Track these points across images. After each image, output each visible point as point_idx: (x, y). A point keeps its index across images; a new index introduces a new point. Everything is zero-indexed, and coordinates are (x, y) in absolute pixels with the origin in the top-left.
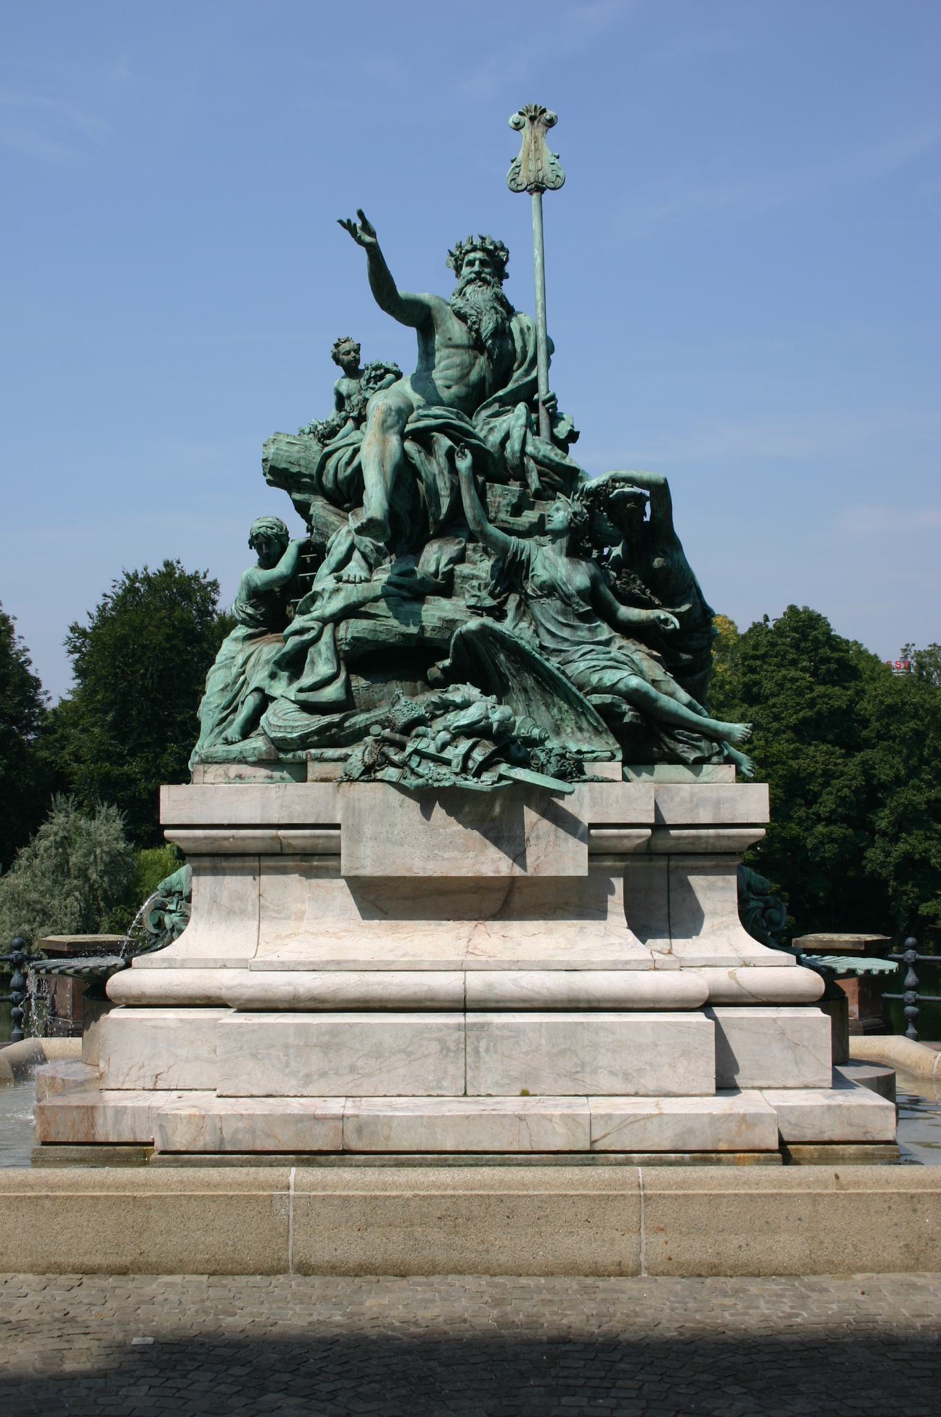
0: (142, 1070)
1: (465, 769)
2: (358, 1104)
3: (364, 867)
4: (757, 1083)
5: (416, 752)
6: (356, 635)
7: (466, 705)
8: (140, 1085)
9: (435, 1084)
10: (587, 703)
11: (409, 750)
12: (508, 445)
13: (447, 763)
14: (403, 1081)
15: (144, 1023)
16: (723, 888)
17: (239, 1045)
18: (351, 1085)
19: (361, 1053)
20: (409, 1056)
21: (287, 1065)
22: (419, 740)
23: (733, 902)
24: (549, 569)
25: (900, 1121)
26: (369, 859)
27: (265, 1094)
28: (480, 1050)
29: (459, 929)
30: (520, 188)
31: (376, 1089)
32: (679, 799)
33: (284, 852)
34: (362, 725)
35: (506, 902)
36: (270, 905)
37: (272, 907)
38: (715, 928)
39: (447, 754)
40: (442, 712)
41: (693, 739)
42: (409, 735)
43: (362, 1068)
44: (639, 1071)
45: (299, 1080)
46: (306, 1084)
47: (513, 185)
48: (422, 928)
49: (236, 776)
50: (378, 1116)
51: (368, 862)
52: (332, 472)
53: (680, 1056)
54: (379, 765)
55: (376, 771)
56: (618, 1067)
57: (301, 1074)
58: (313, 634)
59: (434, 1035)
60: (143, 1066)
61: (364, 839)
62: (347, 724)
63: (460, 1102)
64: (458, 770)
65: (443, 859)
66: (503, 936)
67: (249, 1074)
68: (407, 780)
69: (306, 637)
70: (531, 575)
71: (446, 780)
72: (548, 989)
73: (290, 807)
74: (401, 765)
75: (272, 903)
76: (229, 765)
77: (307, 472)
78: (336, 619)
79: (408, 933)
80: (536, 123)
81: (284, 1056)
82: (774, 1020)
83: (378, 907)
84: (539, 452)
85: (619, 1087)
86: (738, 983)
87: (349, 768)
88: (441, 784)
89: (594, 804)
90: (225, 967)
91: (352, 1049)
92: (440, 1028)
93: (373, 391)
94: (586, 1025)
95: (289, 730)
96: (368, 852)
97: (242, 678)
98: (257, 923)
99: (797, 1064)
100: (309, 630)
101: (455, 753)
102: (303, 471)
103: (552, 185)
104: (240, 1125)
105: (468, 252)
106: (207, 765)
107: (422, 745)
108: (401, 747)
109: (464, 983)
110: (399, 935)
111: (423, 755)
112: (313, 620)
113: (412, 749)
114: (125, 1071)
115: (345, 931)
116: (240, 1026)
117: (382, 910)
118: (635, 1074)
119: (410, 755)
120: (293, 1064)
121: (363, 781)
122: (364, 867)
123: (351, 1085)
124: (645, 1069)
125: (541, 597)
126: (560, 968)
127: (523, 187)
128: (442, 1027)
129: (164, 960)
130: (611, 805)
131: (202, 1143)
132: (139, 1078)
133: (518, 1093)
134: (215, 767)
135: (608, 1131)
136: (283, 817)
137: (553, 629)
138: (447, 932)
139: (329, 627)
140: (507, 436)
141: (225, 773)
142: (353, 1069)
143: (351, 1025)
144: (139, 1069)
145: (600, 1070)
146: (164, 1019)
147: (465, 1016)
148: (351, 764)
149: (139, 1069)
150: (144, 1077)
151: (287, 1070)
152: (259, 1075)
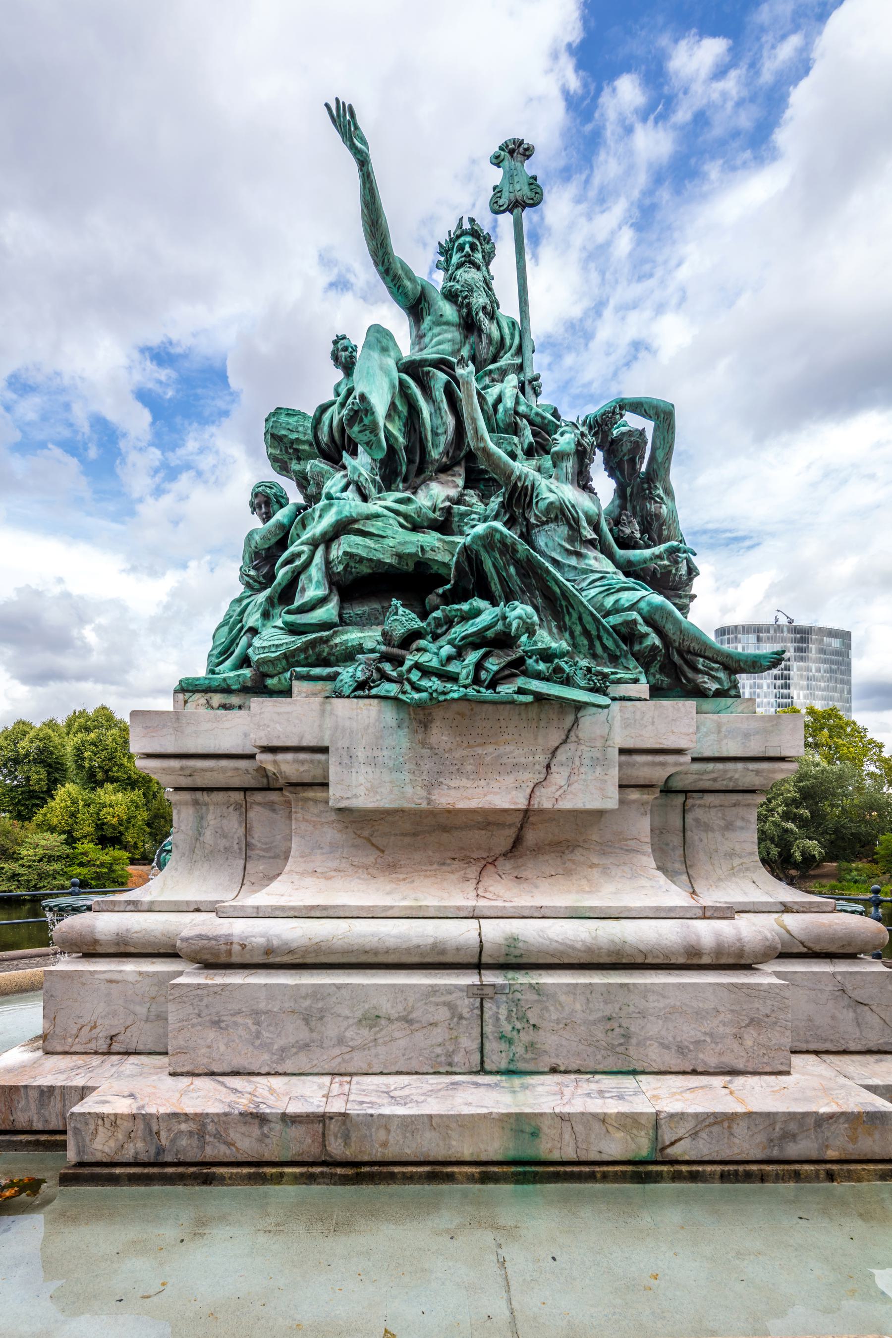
0: (94, 1031)
1: (477, 681)
2: (346, 1087)
3: (356, 796)
4: (812, 1047)
5: (417, 666)
6: (348, 550)
7: (477, 613)
8: (92, 1046)
9: (443, 1059)
10: (606, 624)
11: (408, 664)
12: (501, 408)
13: (453, 678)
14: (404, 1055)
15: (96, 976)
16: (742, 828)
17: (196, 1011)
18: (339, 1059)
19: (351, 1021)
20: (412, 1025)
21: (258, 1035)
22: (419, 654)
23: (753, 842)
24: (556, 491)
25: (487, 1067)
26: (362, 788)
27: (229, 1070)
28: (500, 1016)
29: (466, 868)
30: (502, 208)
31: (370, 1065)
32: (705, 730)
33: (271, 787)
34: (355, 643)
35: (518, 841)
36: (257, 843)
37: (259, 845)
38: (736, 870)
39: (453, 668)
40: (444, 628)
41: (712, 669)
42: (408, 650)
43: (352, 1039)
44: (697, 1043)
45: (273, 1054)
46: (282, 1060)
47: (496, 207)
48: (424, 868)
49: (220, 706)
50: (372, 1115)
51: (361, 791)
52: (327, 423)
53: (748, 1025)
54: (374, 681)
55: (371, 688)
56: (671, 1039)
57: (276, 1047)
58: (304, 557)
59: (443, 999)
60: (95, 1027)
61: (356, 764)
62: (337, 640)
63: (477, 1085)
64: (469, 681)
65: (449, 787)
66: (516, 877)
67: (209, 1047)
68: (407, 695)
69: (298, 563)
70: (534, 501)
71: (454, 691)
72: (582, 941)
73: (268, 726)
74: (399, 681)
75: (259, 841)
76: (212, 695)
77: (305, 439)
78: (329, 539)
79: (407, 873)
80: (515, 155)
81: (254, 1024)
82: (834, 974)
83: (373, 845)
84: (531, 410)
85: (675, 1063)
86: (788, 932)
87: (339, 685)
88: (448, 697)
89: (626, 725)
90: (198, 910)
91: (339, 1016)
92: (450, 990)
93: (367, 1016)
94: (631, 987)
95: (273, 649)
96: (362, 779)
97: (240, 625)
98: (243, 862)
99: (859, 1025)
100: (298, 555)
101: (464, 668)
102: (301, 437)
103: (531, 202)
104: (184, 1127)
105: (458, 237)
106: (188, 695)
107: (423, 658)
108: (398, 662)
109: (480, 934)
110: (398, 876)
111: (426, 672)
112: (302, 544)
113: (412, 662)
114: (74, 1031)
115: (335, 870)
116: (199, 986)
117: (377, 848)
118: (692, 1047)
119: (409, 670)
120: (265, 1034)
121: (355, 697)
122: (356, 796)
123: (339, 1059)
124: (704, 1041)
125: (547, 523)
126: (592, 915)
127: (505, 206)
128: (452, 988)
129: (129, 903)
130: (646, 726)
131: (133, 1151)
132: (90, 1041)
133: (547, 1069)
134: (197, 696)
135: (680, 1135)
136: (261, 738)
137: (559, 558)
138: (452, 872)
139: (320, 553)
140: (499, 400)
141: (208, 702)
142: (341, 1041)
143: (339, 987)
144: (91, 1030)
145: (648, 1042)
146: (121, 972)
147: (480, 974)
148: (342, 680)
149: (91, 1030)
150: (96, 1038)
151: (258, 1042)
152: (222, 1048)
